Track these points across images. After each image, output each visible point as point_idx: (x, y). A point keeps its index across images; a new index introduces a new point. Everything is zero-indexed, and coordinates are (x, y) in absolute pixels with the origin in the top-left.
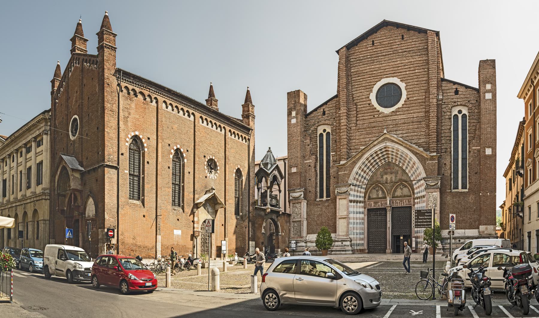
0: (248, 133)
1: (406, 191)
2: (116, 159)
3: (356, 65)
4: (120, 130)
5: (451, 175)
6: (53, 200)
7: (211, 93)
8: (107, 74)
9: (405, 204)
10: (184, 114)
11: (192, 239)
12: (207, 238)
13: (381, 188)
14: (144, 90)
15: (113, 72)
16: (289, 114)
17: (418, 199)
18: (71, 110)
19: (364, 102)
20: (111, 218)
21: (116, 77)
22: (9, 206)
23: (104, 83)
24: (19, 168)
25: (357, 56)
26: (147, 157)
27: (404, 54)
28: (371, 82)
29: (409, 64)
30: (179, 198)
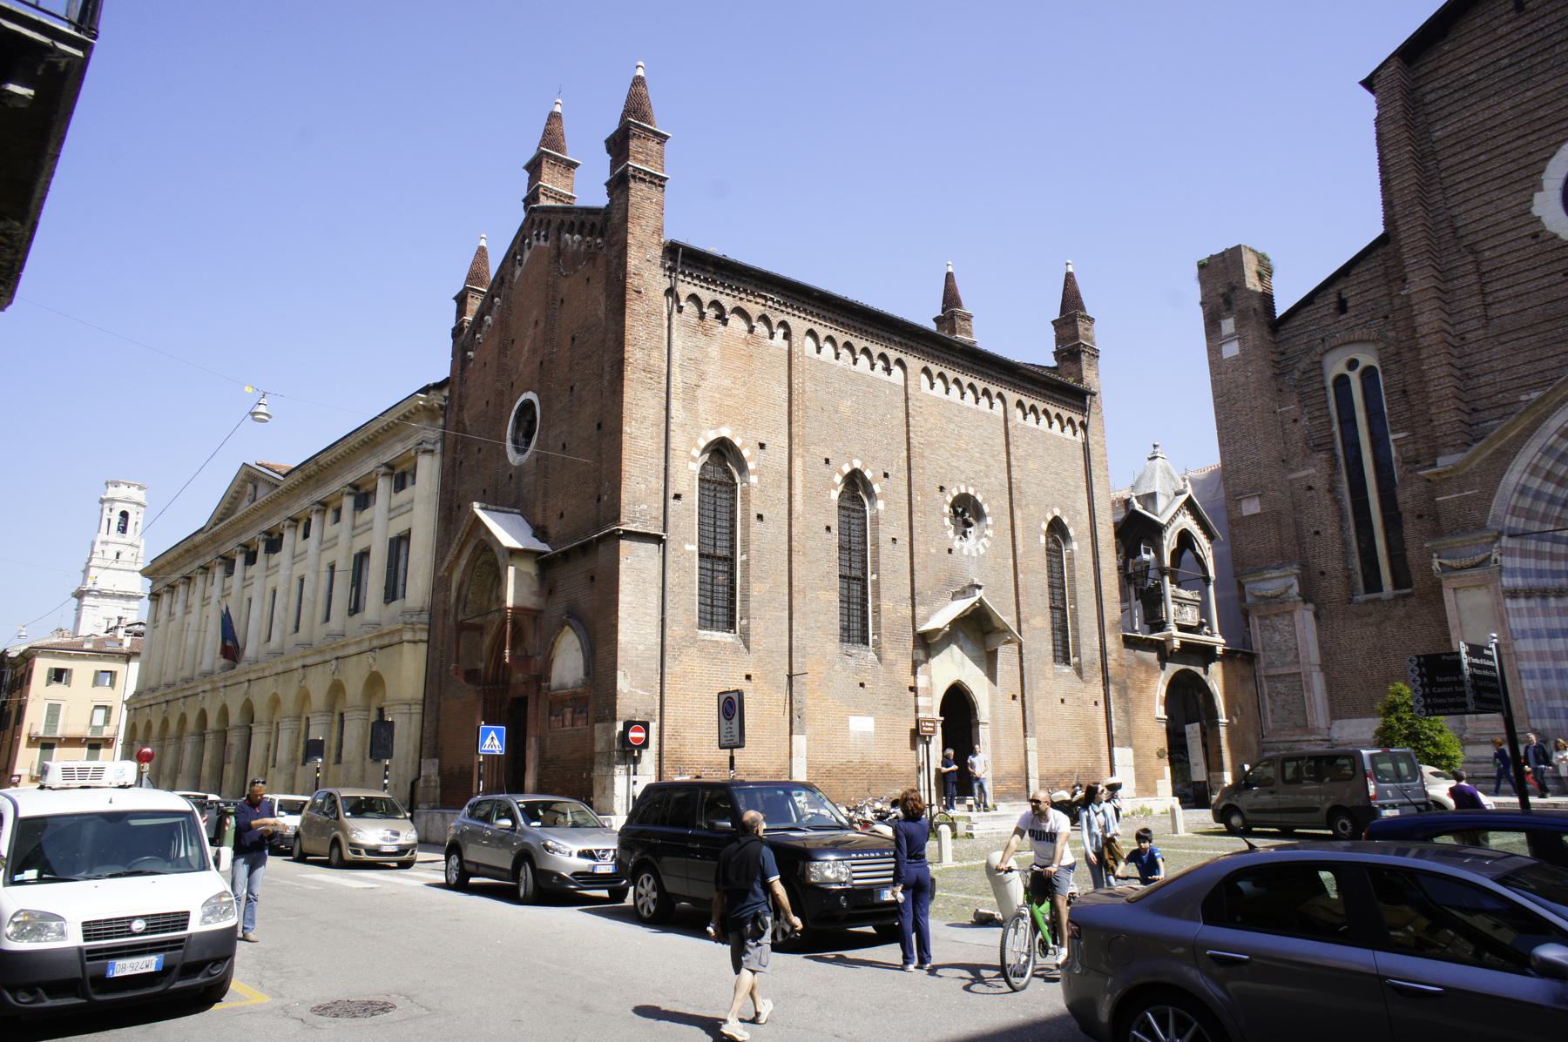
0: (1082, 404)
3: (1450, 109)
4: (672, 427)
7: (951, 298)
11: (914, 746)
19: (1509, 234)
25: (1453, 77)
28: (1530, 153)
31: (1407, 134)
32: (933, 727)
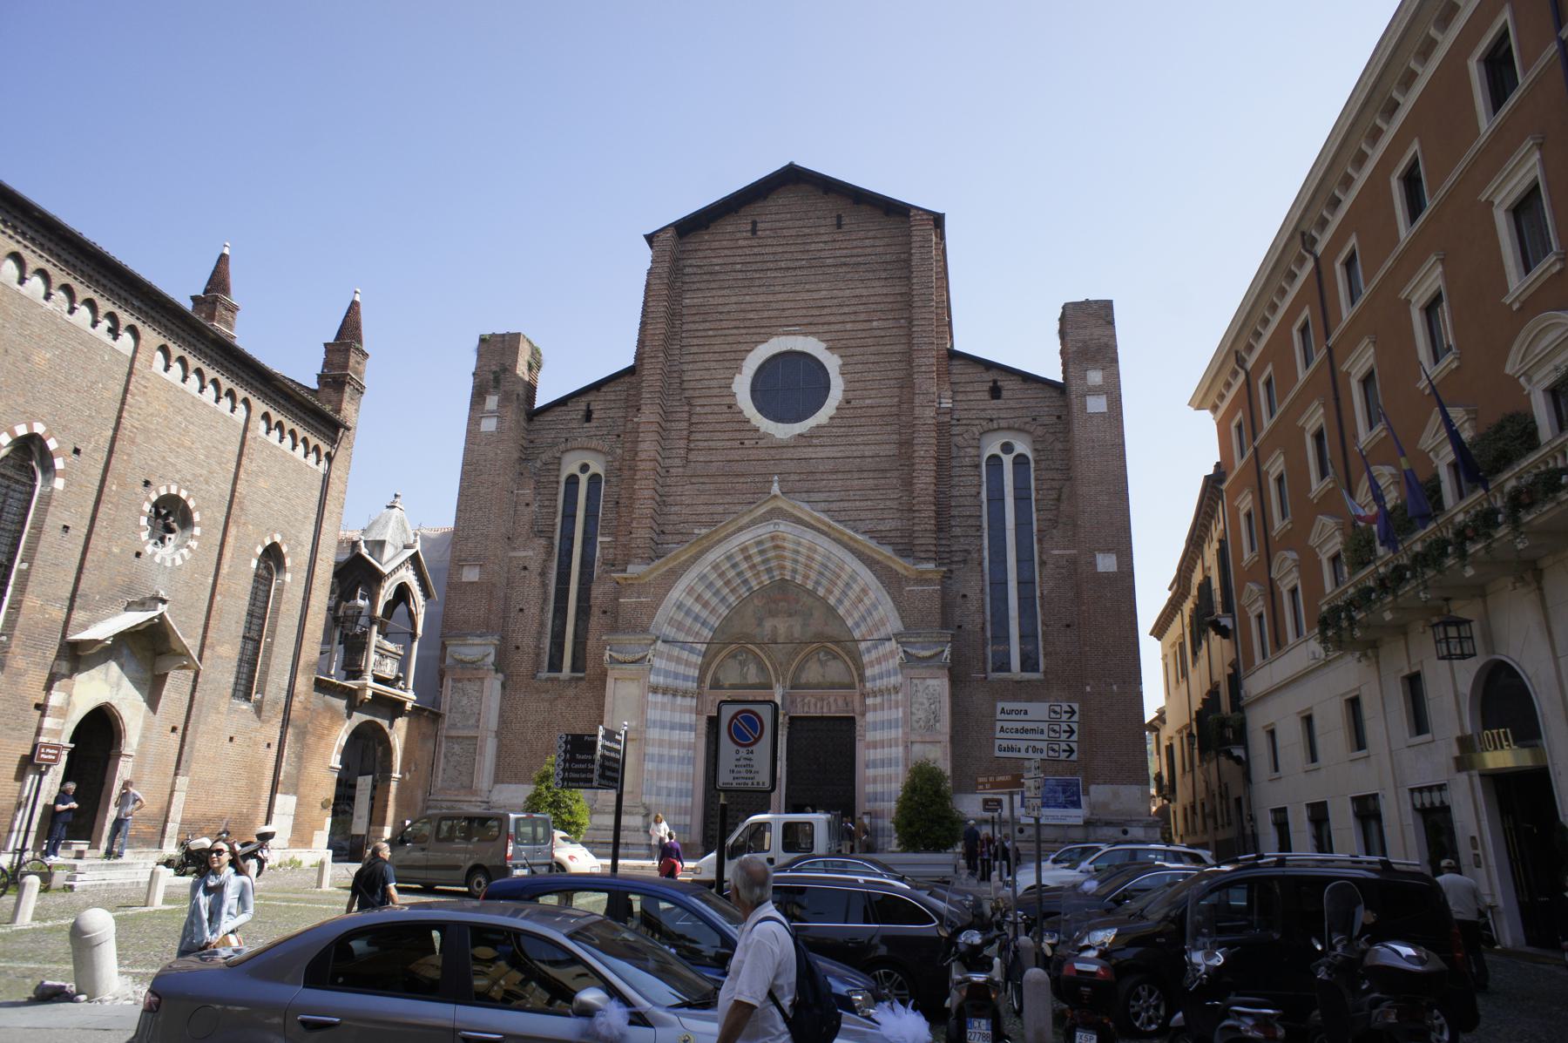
1: (835, 671)
3: (698, 285)
5: (983, 629)
9: (829, 705)
11: (20, 776)
13: (756, 656)
16: (478, 396)
17: (876, 696)
25: (705, 262)
27: (840, 270)
29: (853, 301)
31: (666, 292)
32: (56, 755)
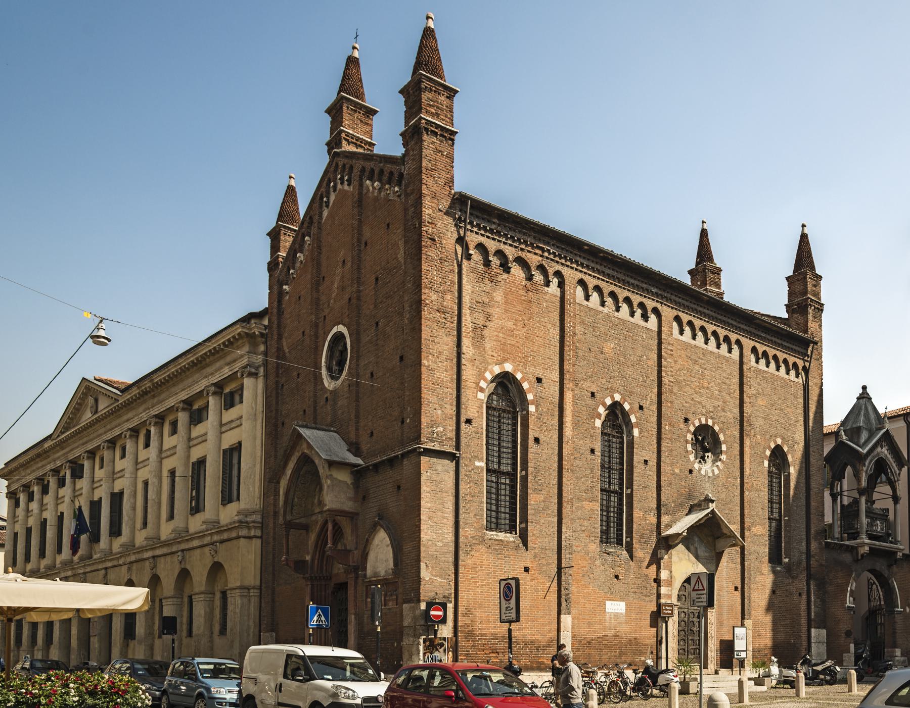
2: (452, 435)
4: (464, 361)
6: (271, 540)
7: (704, 252)
8: (430, 212)
10: (632, 314)
12: (695, 620)
14: (529, 251)
15: (445, 203)
18: (326, 311)
20: (436, 576)
21: (454, 219)
22: (133, 558)
23: (420, 236)
24: (165, 462)
26: (535, 428)
30: (620, 525)
